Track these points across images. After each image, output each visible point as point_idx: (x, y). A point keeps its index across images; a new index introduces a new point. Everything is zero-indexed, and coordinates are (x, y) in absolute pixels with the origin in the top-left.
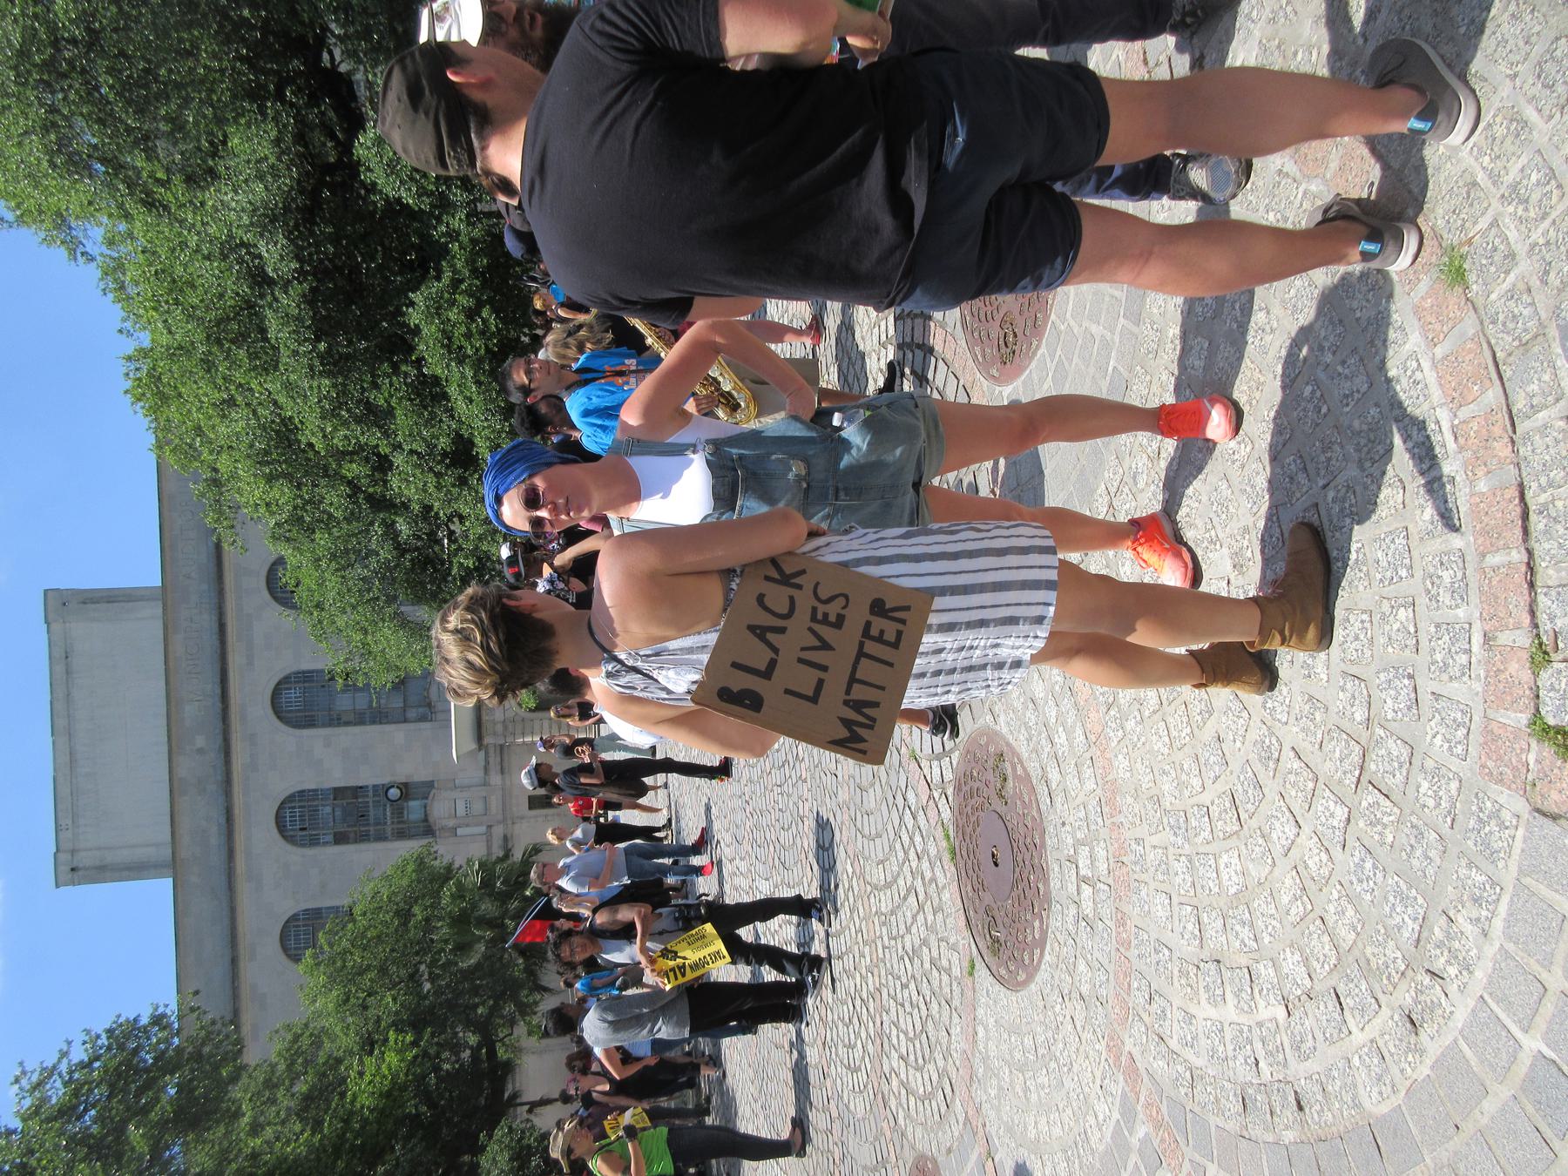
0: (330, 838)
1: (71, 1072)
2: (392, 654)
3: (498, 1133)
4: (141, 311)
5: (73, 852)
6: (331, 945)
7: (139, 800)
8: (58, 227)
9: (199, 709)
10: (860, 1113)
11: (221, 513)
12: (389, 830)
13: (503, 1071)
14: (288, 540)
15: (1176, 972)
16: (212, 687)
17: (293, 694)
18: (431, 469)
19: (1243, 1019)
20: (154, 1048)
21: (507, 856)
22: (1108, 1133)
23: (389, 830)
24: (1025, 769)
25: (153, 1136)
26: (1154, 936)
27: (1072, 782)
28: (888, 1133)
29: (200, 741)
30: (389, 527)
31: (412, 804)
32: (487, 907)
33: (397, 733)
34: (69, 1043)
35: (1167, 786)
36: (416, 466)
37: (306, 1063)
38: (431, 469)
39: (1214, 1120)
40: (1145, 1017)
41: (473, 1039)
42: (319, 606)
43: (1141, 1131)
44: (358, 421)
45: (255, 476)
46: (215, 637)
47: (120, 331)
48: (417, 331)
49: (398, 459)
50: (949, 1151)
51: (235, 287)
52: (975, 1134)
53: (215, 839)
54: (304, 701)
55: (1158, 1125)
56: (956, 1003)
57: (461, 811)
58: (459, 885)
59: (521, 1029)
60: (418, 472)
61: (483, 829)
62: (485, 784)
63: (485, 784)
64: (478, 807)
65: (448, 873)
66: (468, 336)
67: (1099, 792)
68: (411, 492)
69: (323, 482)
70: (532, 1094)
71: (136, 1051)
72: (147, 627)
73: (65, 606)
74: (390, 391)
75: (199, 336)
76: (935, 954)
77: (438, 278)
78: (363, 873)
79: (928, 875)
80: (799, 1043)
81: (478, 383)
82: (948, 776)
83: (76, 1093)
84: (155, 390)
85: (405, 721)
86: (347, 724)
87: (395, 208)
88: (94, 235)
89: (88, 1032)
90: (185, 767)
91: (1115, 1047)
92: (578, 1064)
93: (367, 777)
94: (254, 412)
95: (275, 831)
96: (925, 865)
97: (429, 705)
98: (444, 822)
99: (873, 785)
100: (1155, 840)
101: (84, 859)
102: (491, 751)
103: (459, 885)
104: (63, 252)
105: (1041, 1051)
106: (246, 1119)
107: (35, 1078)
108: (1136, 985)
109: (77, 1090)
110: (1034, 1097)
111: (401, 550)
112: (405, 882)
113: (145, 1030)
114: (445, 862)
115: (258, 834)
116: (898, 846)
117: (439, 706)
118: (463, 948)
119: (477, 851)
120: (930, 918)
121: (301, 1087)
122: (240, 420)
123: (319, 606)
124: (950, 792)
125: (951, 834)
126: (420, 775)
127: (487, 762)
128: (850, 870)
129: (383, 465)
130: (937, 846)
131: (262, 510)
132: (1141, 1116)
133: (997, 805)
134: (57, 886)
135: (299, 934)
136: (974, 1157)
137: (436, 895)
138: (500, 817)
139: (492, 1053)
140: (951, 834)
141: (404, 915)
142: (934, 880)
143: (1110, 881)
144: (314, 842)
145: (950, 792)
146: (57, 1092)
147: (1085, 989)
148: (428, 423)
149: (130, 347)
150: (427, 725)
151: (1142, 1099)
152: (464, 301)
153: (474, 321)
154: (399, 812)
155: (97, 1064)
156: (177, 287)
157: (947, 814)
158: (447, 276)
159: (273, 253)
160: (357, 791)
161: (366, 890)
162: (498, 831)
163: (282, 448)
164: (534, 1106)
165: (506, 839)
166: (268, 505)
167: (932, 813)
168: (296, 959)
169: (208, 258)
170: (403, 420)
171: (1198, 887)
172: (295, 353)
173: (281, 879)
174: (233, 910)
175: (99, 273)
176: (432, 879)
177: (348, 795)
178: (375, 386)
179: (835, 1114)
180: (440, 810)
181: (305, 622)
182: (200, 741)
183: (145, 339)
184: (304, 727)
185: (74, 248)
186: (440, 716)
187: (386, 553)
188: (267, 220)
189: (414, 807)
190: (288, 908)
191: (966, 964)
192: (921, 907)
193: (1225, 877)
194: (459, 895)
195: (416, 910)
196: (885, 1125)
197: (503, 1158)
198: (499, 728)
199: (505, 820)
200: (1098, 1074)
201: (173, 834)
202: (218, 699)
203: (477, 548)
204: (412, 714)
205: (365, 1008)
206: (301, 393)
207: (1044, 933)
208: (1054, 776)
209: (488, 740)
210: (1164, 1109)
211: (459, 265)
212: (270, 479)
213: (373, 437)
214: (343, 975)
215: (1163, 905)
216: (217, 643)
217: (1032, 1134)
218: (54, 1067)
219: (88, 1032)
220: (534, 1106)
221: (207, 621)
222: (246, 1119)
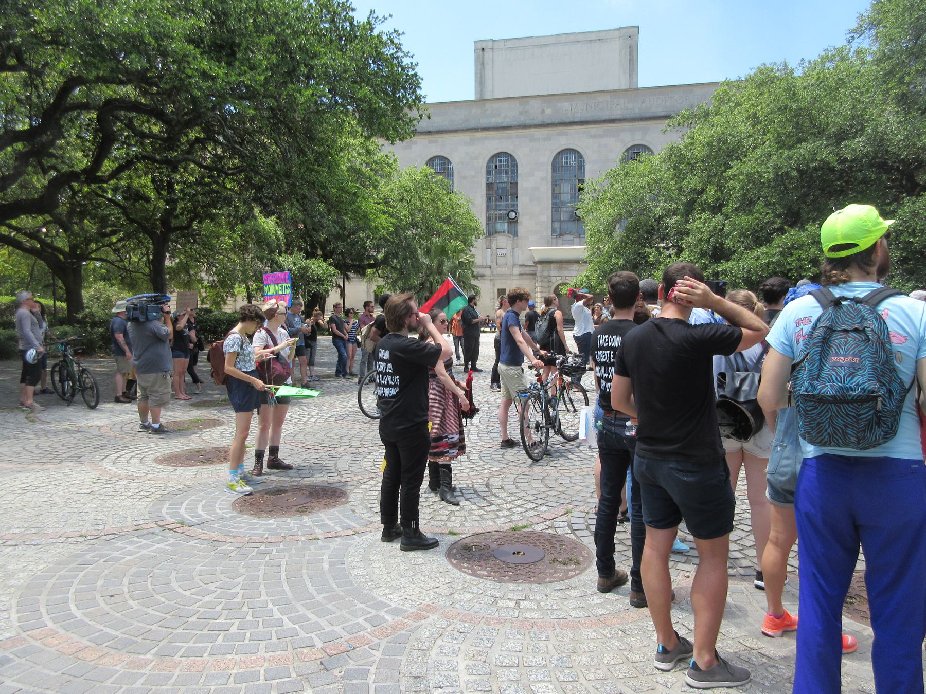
0: (490, 181)
1: (398, 57)
3: (332, 269)
4: (817, 71)
5: (492, 49)
7: (511, 82)
8: (871, 23)
9: (567, 110)
10: (365, 464)
11: (688, 118)
13: (361, 271)
15: (479, 649)
16: (578, 117)
17: (571, 160)
18: (712, 236)
19: (462, 684)
20: (404, 97)
21: (474, 276)
22: (383, 599)
24: (573, 577)
25: (365, 98)
26: (496, 639)
27: (572, 604)
28: (356, 478)
29: (548, 111)
30: (675, 213)
31: (506, 224)
32: (448, 264)
33: (546, 216)
34: (412, 57)
35: (584, 659)
36: (715, 228)
37: (376, 171)
38: (712, 236)
39: (404, 659)
40: (450, 628)
41: (380, 256)
42: (627, 174)
43: (388, 617)
44: (744, 195)
45: (712, 136)
46: (607, 117)
47: (803, 59)
48: (803, 229)
49: (719, 218)
50: (354, 511)
51: (836, 122)
52: (365, 526)
53: (494, 121)
54: (567, 166)
55: (394, 628)
56: (432, 522)
57: (500, 251)
59: (381, 282)
60: (711, 228)
61: (489, 263)
62: (514, 266)
63: (514, 266)
64: (501, 261)
66: (799, 259)
67: (570, 619)
68: (693, 226)
69: (705, 174)
70: (348, 288)
71: (404, 88)
72: (618, 82)
73: (629, 39)
74: (762, 214)
75: (802, 105)
76: (457, 513)
78: (471, 197)
79: (500, 514)
81: (768, 264)
82: (560, 531)
83: (386, 61)
84: (764, 80)
85: (553, 221)
86: (553, 190)
88: (867, 44)
89: (417, 64)
90: (535, 105)
91: (430, 609)
93: (523, 201)
94: (750, 136)
95: (496, 152)
96: (506, 513)
97: (561, 235)
98: (494, 242)
99: (546, 486)
100: (551, 647)
101: (488, 55)
102: (533, 269)
103: (462, 251)
104: (854, 25)
105: (417, 567)
106: (352, 141)
107: (396, 41)
108: (467, 625)
109: (388, 61)
110: (392, 561)
111: (660, 219)
112: (465, 221)
113: (414, 92)
114: (475, 243)
115: (494, 144)
116: (513, 498)
117: (560, 240)
118: (428, 252)
119: (478, 260)
120: (476, 513)
121: (366, 170)
122: (744, 128)
123: (627, 174)
124: (550, 531)
125: (526, 530)
126: (521, 229)
127: (526, 266)
128: (494, 469)
129: (716, 208)
130: (518, 520)
131: (689, 141)
132: (396, 619)
133: (548, 558)
134: (475, 42)
136: (353, 524)
137: (457, 237)
138: (495, 273)
140: (526, 530)
142: (498, 517)
143: (520, 618)
144: (489, 172)
145: (550, 531)
146: (388, 51)
147: (456, 596)
148: (742, 234)
149: (792, 65)
150: (550, 233)
151: (406, 620)
153: (809, 262)
154: (501, 218)
155: (400, 69)
156: (832, 92)
157: (538, 528)
159: (858, 145)
161: (462, 201)
162: (487, 272)
163: (725, 153)
165: (483, 276)
166: (692, 144)
167: (536, 520)
168: (428, 163)
169: (854, 107)
171: (531, 669)
172: (790, 158)
173: (470, 158)
174: (456, 131)
175: (839, 46)
176: (465, 234)
179: (360, 450)
180: (502, 240)
181: (615, 165)
182: (548, 111)
183: (798, 73)
184: (553, 167)
185: (859, 31)
186: (554, 240)
187: (658, 211)
188: (880, 141)
190: (455, 160)
191: (455, 530)
192: (481, 508)
193: (540, 685)
194: (457, 251)
195: (450, 227)
196: (360, 477)
197: (319, 272)
198: (546, 274)
199: (494, 275)
200: (413, 598)
201: (499, 99)
202: (571, 120)
203: (660, 263)
204: (557, 225)
205: (402, 200)
206: (761, 162)
207: (481, 576)
208: (573, 593)
209: (539, 267)
210: (403, 632)
212: (709, 144)
213: (732, 204)
214: (420, 187)
215: (515, 647)
216: (604, 118)
217: (372, 557)
218: (400, 49)
219: (417, 64)
221: (617, 113)
222: (352, 141)
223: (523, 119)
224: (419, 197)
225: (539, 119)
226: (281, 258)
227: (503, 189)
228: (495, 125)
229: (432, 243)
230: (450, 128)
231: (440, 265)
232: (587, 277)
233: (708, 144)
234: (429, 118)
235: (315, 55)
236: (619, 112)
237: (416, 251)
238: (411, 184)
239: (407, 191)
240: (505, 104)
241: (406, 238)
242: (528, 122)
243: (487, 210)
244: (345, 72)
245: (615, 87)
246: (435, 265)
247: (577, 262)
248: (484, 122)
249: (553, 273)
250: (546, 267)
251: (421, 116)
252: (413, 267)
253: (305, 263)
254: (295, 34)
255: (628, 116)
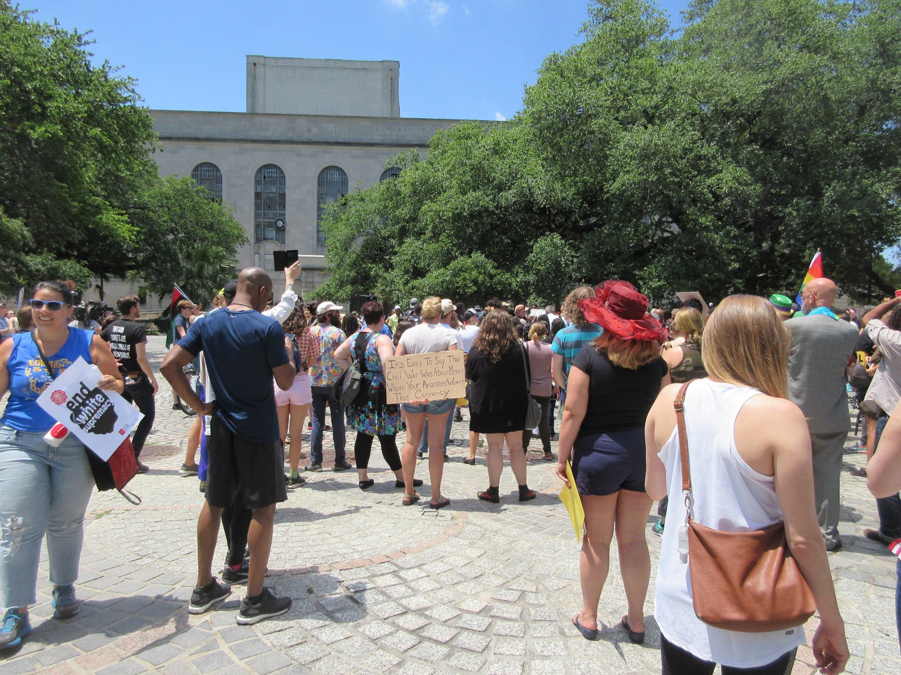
0: (259, 190)
2: (336, 232)
3: (86, 270)
5: (264, 65)
6: (197, 192)
9: (332, 131)
12: (261, 220)
13: (120, 273)
14: (388, 189)
23: (261, 220)
29: (315, 130)
31: (274, 232)
46: (368, 141)
53: (262, 135)
54: (331, 182)
58: (223, 257)
59: (143, 283)
65: (231, 251)
66: (465, 279)
70: (107, 287)
72: (379, 109)
77: (494, 267)
80: (175, 473)
84: (467, 132)
87: (528, 250)
90: (302, 124)
92: (229, 295)
93: (290, 211)
101: (260, 70)
103: (223, 257)
112: (228, 229)
115: (264, 156)
118: (188, 257)
129: (419, 234)
135: (208, 174)
137: (218, 244)
139: (131, 268)
141: (211, 228)
144: (257, 182)
152: (481, 277)
154: (270, 225)
158: (493, 272)
159: (509, 196)
160: (283, 205)
163: (427, 191)
164: (100, 288)
170: (433, 246)
173: (238, 170)
177: (281, 200)
178: (449, 236)
182: (315, 130)
186: (320, 249)
187: (385, 233)
189: (272, 233)
194: (220, 258)
198: (310, 280)
202: (336, 140)
211: (498, 277)
212: (413, 184)
216: (365, 142)
220: (100, 288)
221: (377, 138)
223: (290, 135)
224: (179, 205)
225: (306, 137)
226: (28, 258)
227: (271, 199)
228: (263, 138)
229: (193, 248)
230: (219, 136)
231: (201, 268)
232: (328, 286)
233: (412, 184)
234: (162, 151)
235: (50, 97)
236: (379, 137)
237: (176, 255)
238: (171, 192)
239: (167, 198)
240: (274, 120)
241: (166, 243)
242: (295, 138)
243: (256, 218)
244: (78, 113)
245: (379, 114)
246: (195, 269)
247: (321, 269)
248: (253, 135)
249: (316, 279)
250: (310, 274)
251: (154, 149)
252: (172, 270)
253: (55, 264)
254: (31, 77)
255: (386, 142)
